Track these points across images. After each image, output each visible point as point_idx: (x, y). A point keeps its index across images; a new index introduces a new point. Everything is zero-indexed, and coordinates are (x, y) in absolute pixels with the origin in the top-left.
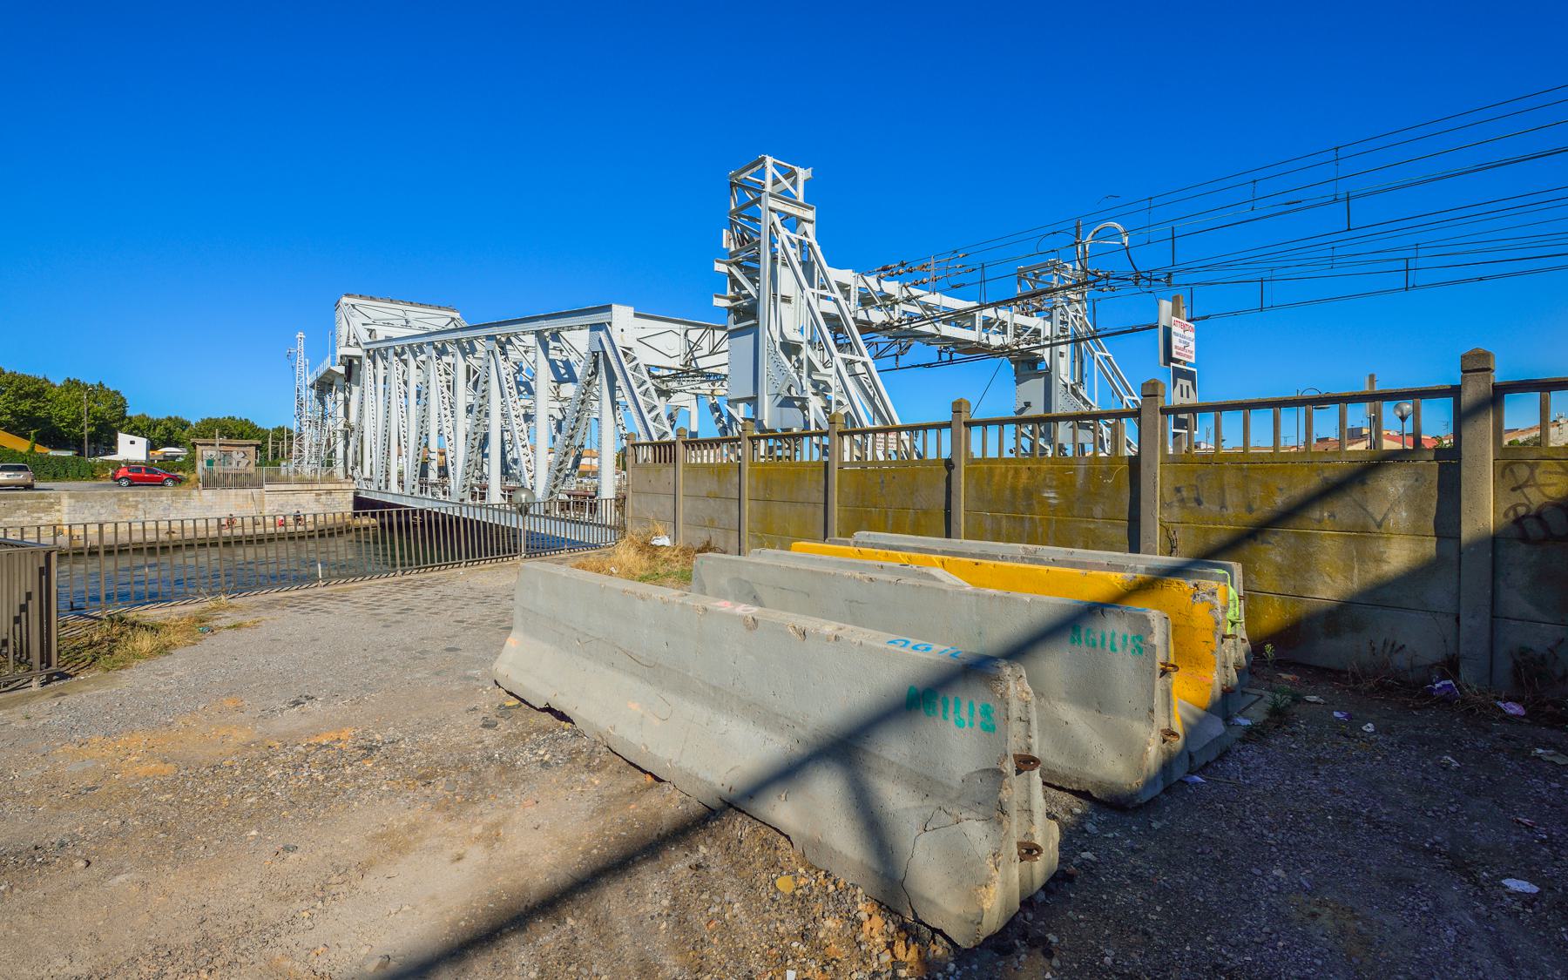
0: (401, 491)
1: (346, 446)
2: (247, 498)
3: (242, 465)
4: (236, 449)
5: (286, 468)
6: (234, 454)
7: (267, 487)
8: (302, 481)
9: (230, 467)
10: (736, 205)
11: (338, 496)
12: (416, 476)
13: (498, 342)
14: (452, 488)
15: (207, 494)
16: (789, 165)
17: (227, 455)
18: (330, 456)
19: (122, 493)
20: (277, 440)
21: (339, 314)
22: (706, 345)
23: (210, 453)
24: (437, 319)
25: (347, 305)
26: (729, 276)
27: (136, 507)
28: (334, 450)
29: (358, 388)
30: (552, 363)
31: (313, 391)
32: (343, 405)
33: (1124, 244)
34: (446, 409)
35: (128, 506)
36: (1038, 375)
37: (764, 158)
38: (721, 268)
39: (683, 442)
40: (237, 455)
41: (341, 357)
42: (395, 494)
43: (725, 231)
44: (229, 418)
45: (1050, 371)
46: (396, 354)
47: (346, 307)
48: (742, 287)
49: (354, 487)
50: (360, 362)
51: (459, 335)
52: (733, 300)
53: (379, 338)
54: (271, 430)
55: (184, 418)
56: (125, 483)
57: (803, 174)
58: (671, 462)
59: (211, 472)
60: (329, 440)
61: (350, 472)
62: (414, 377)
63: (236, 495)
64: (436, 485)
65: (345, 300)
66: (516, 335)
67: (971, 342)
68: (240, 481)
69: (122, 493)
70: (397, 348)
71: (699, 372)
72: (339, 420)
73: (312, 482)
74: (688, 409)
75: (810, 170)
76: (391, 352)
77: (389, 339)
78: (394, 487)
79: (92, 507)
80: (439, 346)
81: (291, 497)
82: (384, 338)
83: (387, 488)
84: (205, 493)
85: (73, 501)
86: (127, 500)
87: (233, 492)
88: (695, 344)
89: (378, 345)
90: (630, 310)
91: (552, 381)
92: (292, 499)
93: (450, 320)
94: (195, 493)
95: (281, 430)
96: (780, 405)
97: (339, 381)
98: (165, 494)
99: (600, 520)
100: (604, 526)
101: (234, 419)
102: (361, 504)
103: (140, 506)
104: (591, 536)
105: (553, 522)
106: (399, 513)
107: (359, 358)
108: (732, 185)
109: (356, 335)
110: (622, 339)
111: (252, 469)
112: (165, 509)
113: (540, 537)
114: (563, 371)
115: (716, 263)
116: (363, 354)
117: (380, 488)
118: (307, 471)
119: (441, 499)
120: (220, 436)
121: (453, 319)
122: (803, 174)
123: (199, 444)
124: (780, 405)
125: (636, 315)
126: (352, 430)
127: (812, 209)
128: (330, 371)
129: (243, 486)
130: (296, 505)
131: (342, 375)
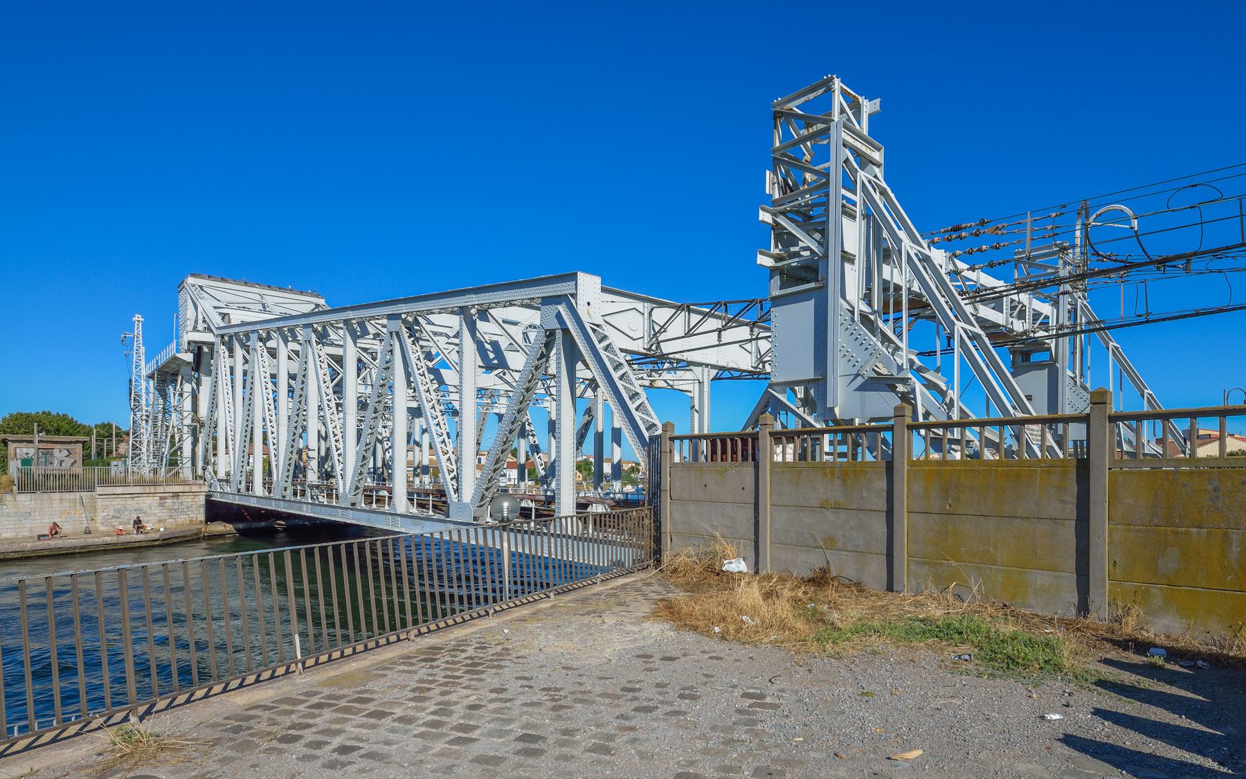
0: (267, 494)
1: (195, 442)
2: (75, 503)
3: (66, 465)
4: (59, 446)
5: (116, 468)
6: (56, 452)
7: (99, 490)
8: (141, 482)
9: (50, 467)
10: (780, 142)
11: (187, 500)
12: (288, 477)
13: (405, 321)
14: (341, 490)
15: (25, 499)
16: (854, 93)
17: (48, 453)
18: (175, 453)
20: (100, 439)
21: (184, 296)
22: (677, 328)
23: (25, 450)
24: (300, 304)
25: (193, 286)
26: (773, 229)
28: (180, 448)
29: (209, 378)
31: (151, 383)
32: (190, 396)
33: (1132, 228)
34: (329, 401)
36: (1039, 366)
37: (831, 79)
38: (765, 217)
39: (771, 434)
40: (59, 453)
41: (189, 343)
42: (261, 498)
43: (768, 172)
44: (44, 413)
45: (1056, 361)
46: (261, 339)
47: (193, 289)
48: (794, 240)
49: (206, 489)
50: (212, 350)
52: (778, 258)
53: (233, 322)
54: (93, 426)
57: (868, 107)
59: (28, 474)
60: (173, 437)
61: (200, 472)
62: (285, 366)
63: (61, 500)
64: (317, 487)
65: (191, 280)
67: (999, 325)
68: (66, 484)
70: (261, 332)
71: (663, 357)
72: (185, 414)
73: (154, 483)
74: (548, 410)
76: (254, 337)
77: (243, 324)
78: (259, 489)
80: (320, 329)
81: (130, 502)
83: (248, 489)
87: (57, 496)
88: (662, 327)
89: (237, 330)
90: (597, 281)
91: (480, 367)
92: (132, 503)
94: (9, 497)
95: (103, 426)
97: (185, 370)
99: (558, 529)
100: (564, 536)
101: (49, 414)
102: (215, 511)
104: (586, 555)
105: (552, 540)
106: (384, 543)
107: (211, 345)
108: (777, 115)
109: (207, 319)
110: (589, 314)
111: (78, 469)
113: (444, 547)
114: (492, 356)
115: (761, 212)
116: (217, 341)
117: (239, 490)
118: (146, 471)
119: (326, 503)
120: (39, 432)
122: (868, 107)
123: (11, 441)
124: (861, 388)
125: (604, 290)
126: (202, 425)
127: (879, 150)
128: (175, 358)
129: (69, 489)
130: (137, 510)
131: (189, 363)
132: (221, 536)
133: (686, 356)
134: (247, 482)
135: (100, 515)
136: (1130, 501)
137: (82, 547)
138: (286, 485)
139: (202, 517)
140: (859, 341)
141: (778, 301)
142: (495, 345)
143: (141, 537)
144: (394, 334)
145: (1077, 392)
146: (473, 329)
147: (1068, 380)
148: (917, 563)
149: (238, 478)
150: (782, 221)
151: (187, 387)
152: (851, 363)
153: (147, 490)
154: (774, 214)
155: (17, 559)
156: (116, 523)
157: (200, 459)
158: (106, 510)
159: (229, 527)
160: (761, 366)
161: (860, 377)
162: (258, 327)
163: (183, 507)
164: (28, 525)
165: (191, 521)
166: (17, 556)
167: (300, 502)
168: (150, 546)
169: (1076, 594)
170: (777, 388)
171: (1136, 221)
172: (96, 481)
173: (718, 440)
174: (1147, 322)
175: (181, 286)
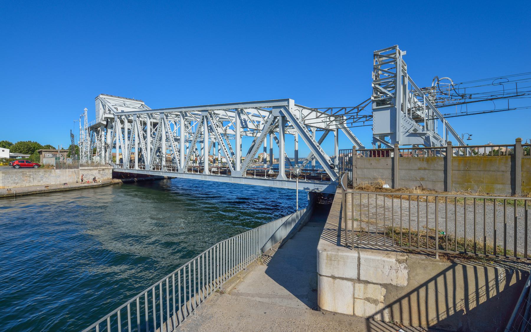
7: (80, 168)
11: (106, 171)
19: (24, 171)
21: (98, 102)
23: (48, 155)
27: (30, 177)
30: (241, 120)
35: (26, 177)
41: (105, 118)
44: (29, 141)
51: (149, 112)
52: (375, 98)
55: (9, 141)
56: (17, 167)
57: (403, 53)
63: (69, 171)
65: (101, 96)
66: (170, 113)
69: (24, 171)
75: (405, 51)
78: (137, 167)
79: (12, 177)
81: (89, 172)
82: (121, 112)
84: (57, 170)
85: (4, 174)
86: (26, 174)
87: (67, 170)
93: (141, 105)
94: (53, 170)
96: (408, 136)
98: (41, 171)
101: (31, 142)
102: (116, 175)
103: (31, 176)
108: (375, 55)
112: (41, 177)
114: (244, 124)
121: (142, 105)
125: (295, 105)
132: (118, 183)
133: (312, 125)
134: (130, 165)
136: (528, 166)
137: (78, 187)
138: (151, 166)
139: (111, 177)
140: (408, 122)
142: (245, 120)
143: (96, 184)
144: (204, 116)
146: (239, 117)
149: (127, 164)
150: (377, 86)
151: (103, 133)
152: (405, 129)
153: (95, 168)
154: (374, 84)
155: (59, 191)
157: (107, 157)
159: (120, 181)
160: (328, 127)
162: (137, 113)
164: (59, 180)
165: (108, 178)
166: (59, 190)
167: (160, 172)
169: (511, 190)
173: (385, 151)
174: (467, 115)
175: (97, 98)
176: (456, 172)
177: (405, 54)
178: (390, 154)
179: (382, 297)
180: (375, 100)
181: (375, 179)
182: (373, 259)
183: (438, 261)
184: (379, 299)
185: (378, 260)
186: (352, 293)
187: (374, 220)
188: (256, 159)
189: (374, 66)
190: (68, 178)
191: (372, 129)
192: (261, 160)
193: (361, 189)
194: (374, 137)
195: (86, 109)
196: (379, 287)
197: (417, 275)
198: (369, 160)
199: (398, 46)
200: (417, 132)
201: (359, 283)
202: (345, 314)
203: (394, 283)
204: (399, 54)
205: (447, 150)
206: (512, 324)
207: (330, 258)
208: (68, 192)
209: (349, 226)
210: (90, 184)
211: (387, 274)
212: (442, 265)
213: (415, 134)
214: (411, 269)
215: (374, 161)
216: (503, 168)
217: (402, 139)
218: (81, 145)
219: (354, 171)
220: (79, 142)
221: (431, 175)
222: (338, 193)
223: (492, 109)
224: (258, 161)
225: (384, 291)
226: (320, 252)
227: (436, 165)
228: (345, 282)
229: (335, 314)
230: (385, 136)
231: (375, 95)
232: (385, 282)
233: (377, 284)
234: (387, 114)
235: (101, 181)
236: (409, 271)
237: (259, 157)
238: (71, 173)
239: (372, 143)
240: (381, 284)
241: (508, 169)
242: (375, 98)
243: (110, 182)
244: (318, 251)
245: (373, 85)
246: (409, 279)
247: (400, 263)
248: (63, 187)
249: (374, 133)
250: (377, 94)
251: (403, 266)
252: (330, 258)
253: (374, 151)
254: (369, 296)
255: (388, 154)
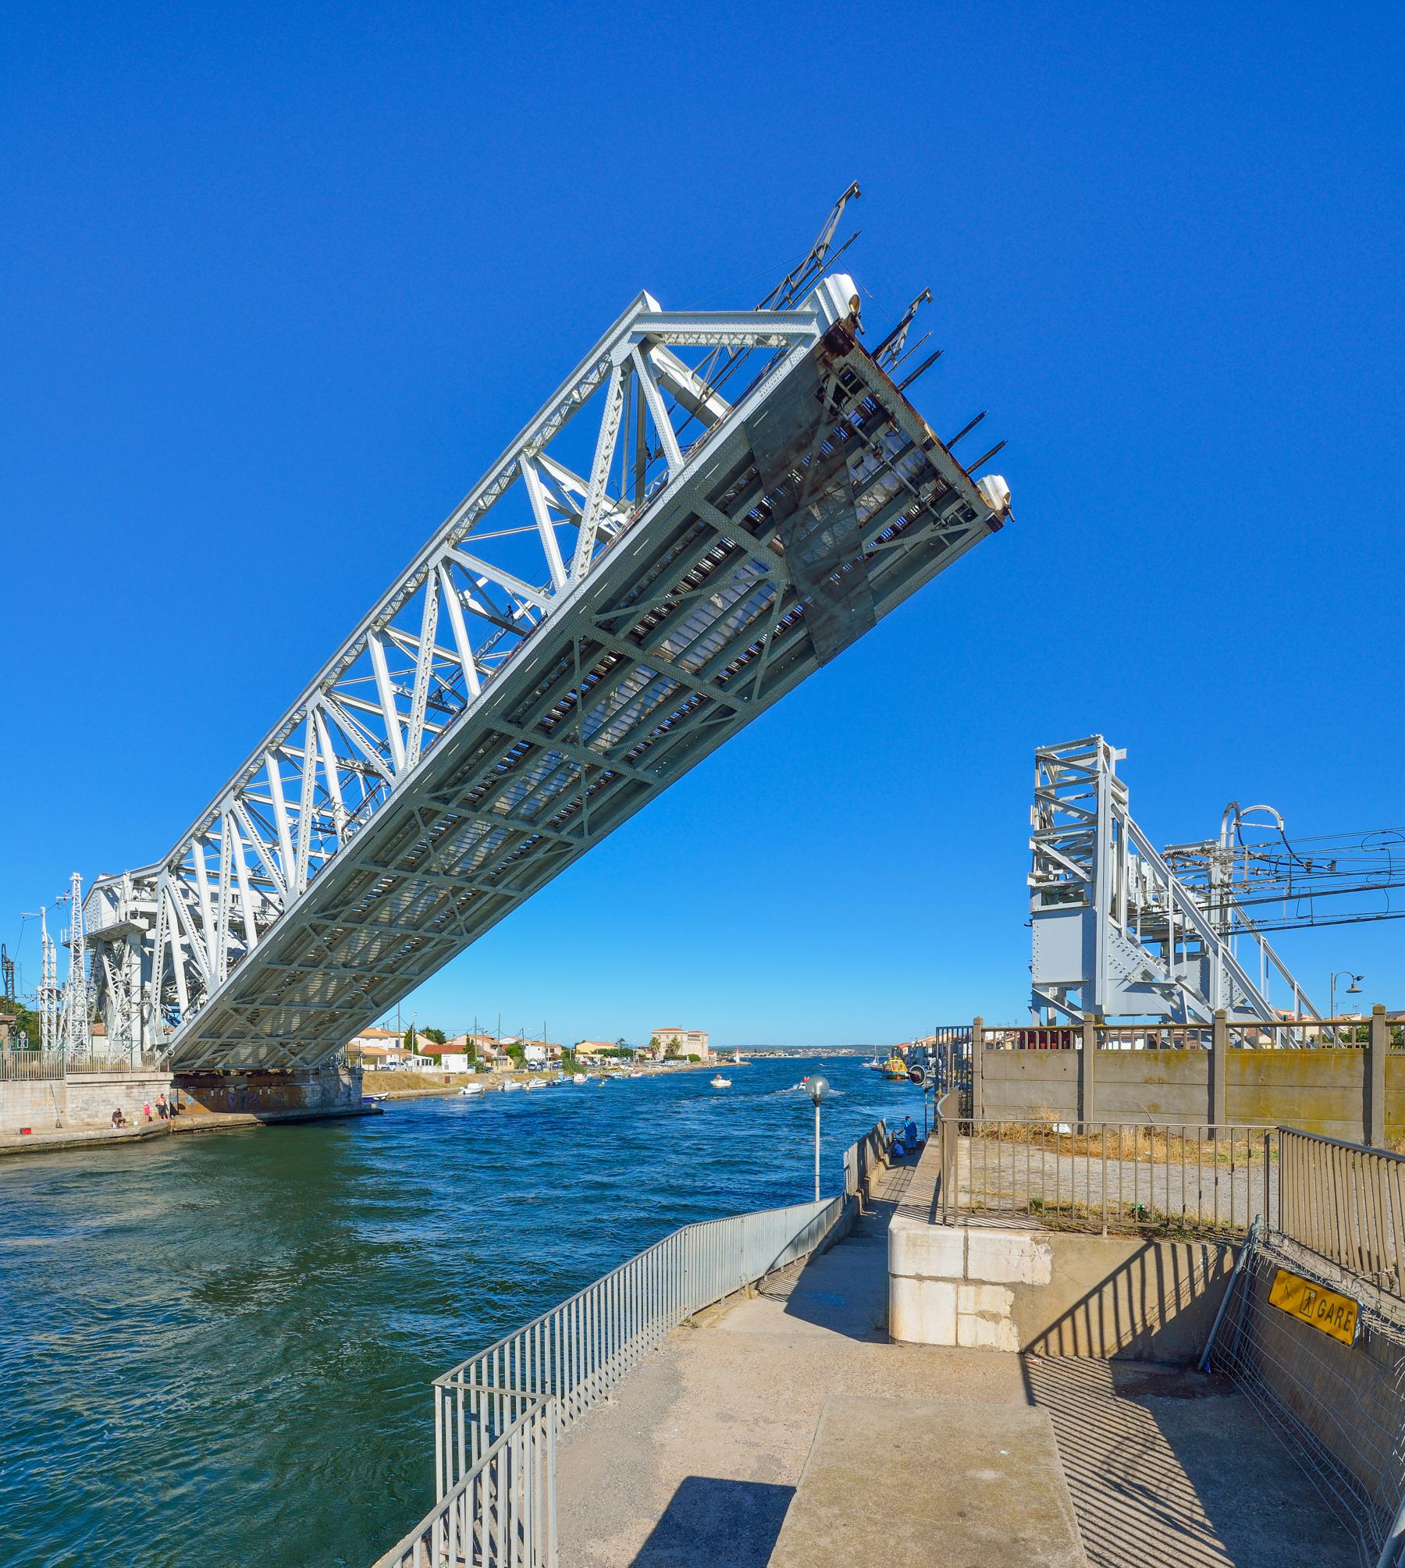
7: (69, 1078)
52: (1039, 879)
57: (1117, 754)
58: (554, 1392)
75: (1124, 751)
81: (98, 1091)
87: (28, 1084)
96: (1127, 990)
108: (1038, 759)
127: (1124, 790)
135: (70, 1107)
136: (1400, 1075)
137: (68, 1142)
141: (1038, 915)
143: (121, 1132)
145: (1123, 947)
147: (1110, 930)
148: (1234, 1120)
150: (1045, 848)
153: (115, 1077)
154: (1037, 842)
156: (84, 1115)
158: (75, 1101)
161: (1126, 982)
163: (149, 1097)
168: (131, 1142)
170: (1038, 987)
171: (1282, 822)
172: (65, 1068)
176: (1237, 1089)
177: (1124, 756)
178: (1072, 1042)
179: (1008, 1308)
180: (1039, 888)
181: (1033, 1108)
182: (991, 1240)
183: (1105, 1239)
184: (1001, 1311)
185: (1000, 1240)
186: (953, 1304)
187: (1010, 1192)
188: (643, 1048)
189: (1036, 789)
190: (30, 1111)
191: (1030, 968)
192: (663, 1053)
193: (994, 1135)
194: (1034, 993)
195: (76, 876)
196: (1002, 1289)
197: (1066, 1262)
198: (1018, 1056)
199: (1102, 738)
200: (1154, 981)
201: (967, 1285)
202: (940, 1346)
203: (1028, 1281)
204: (1107, 756)
205: (1214, 1030)
206: (1216, 1335)
207: (913, 1242)
208: (34, 1156)
209: (951, 1201)
210: (106, 1133)
211: (1015, 1265)
212: (1109, 1243)
213: (1144, 986)
214: (1056, 1252)
215: (1031, 1058)
216: (1344, 1080)
217: (1111, 998)
218: (45, 997)
219: (978, 1087)
220: (40, 989)
221: (1175, 1098)
222: (931, 1146)
223: (1380, 909)
224: (649, 1056)
225: (1010, 1296)
226: (895, 1231)
227: (1187, 1072)
228: (941, 1284)
229: (922, 1345)
230: (1067, 989)
231: (1039, 873)
232: (1013, 1279)
233: (998, 1284)
234: (1074, 925)
235: (136, 1123)
236: (1054, 1257)
237: (655, 1042)
238: (38, 1095)
239: (1030, 1008)
240: (1004, 1284)
241: (1355, 1082)
242: (1039, 879)
243: (166, 1126)
244: (891, 1232)
245: (1033, 846)
246: (1053, 1272)
247: (1037, 1243)
248: (19, 1140)
249: (1037, 981)
250: (1045, 869)
251: (1042, 1248)
252: (913, 1242)
253: (1032, 1033)
254: (984, 1307)
255: (1068, 1042)
